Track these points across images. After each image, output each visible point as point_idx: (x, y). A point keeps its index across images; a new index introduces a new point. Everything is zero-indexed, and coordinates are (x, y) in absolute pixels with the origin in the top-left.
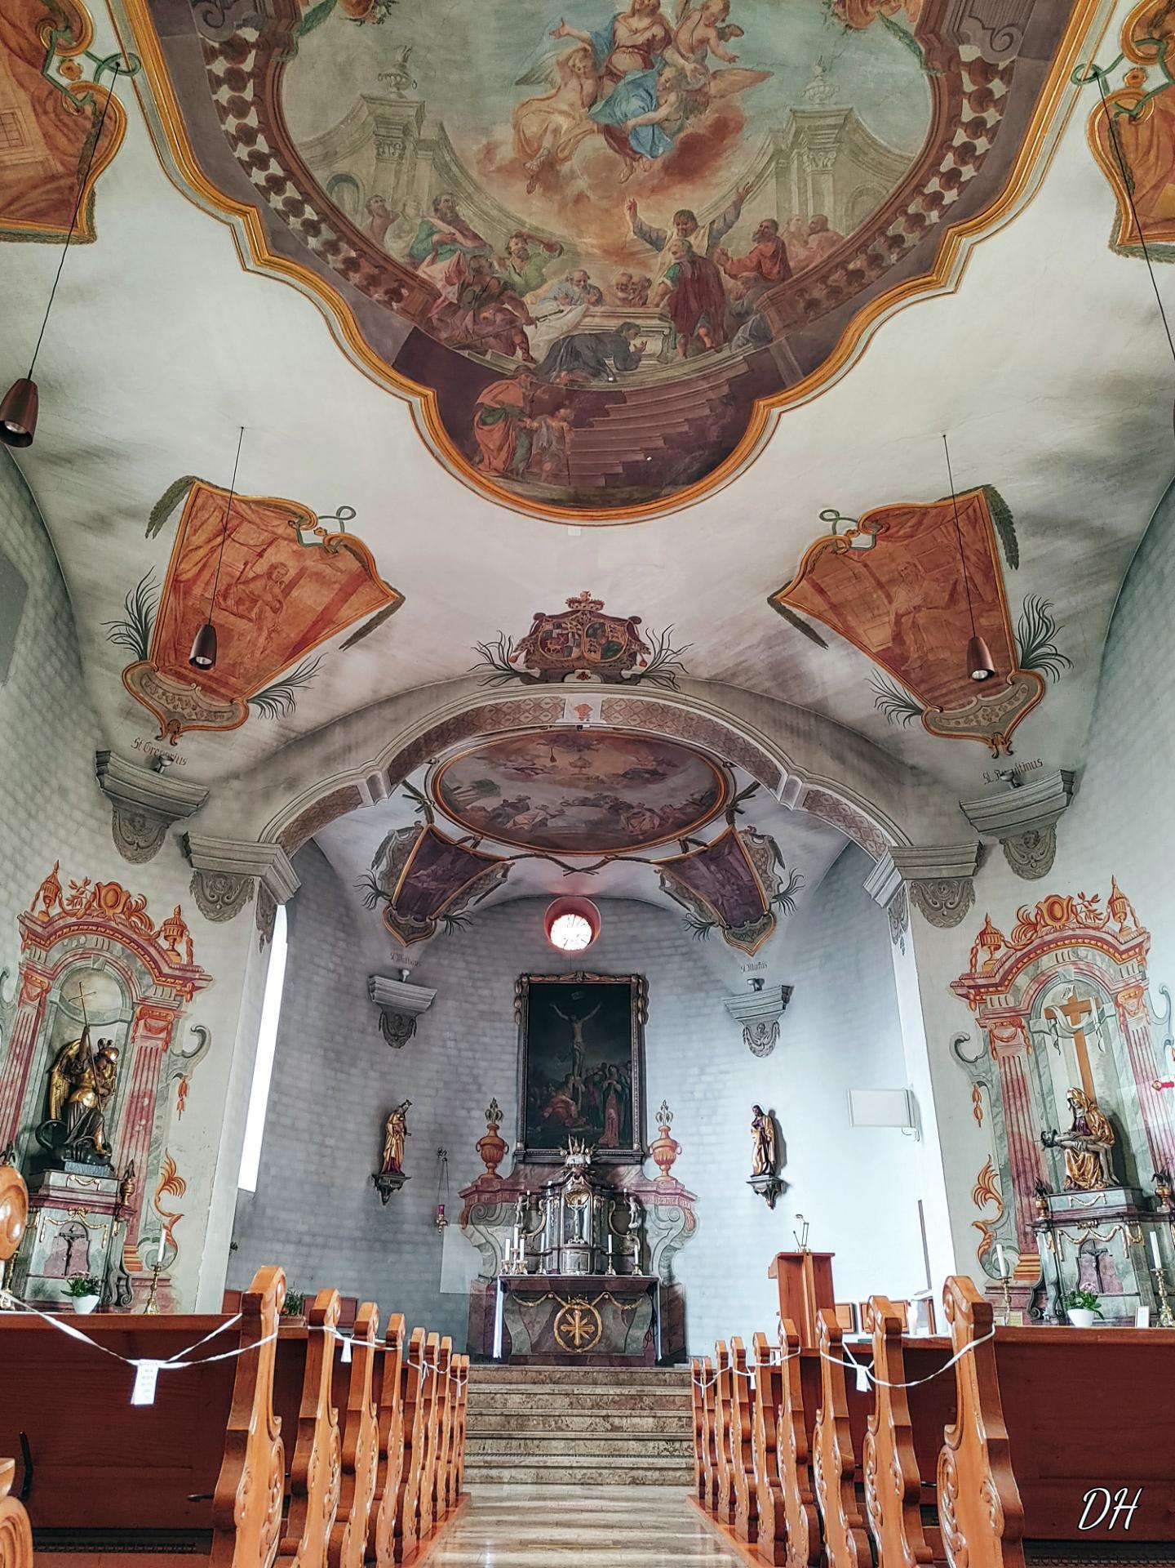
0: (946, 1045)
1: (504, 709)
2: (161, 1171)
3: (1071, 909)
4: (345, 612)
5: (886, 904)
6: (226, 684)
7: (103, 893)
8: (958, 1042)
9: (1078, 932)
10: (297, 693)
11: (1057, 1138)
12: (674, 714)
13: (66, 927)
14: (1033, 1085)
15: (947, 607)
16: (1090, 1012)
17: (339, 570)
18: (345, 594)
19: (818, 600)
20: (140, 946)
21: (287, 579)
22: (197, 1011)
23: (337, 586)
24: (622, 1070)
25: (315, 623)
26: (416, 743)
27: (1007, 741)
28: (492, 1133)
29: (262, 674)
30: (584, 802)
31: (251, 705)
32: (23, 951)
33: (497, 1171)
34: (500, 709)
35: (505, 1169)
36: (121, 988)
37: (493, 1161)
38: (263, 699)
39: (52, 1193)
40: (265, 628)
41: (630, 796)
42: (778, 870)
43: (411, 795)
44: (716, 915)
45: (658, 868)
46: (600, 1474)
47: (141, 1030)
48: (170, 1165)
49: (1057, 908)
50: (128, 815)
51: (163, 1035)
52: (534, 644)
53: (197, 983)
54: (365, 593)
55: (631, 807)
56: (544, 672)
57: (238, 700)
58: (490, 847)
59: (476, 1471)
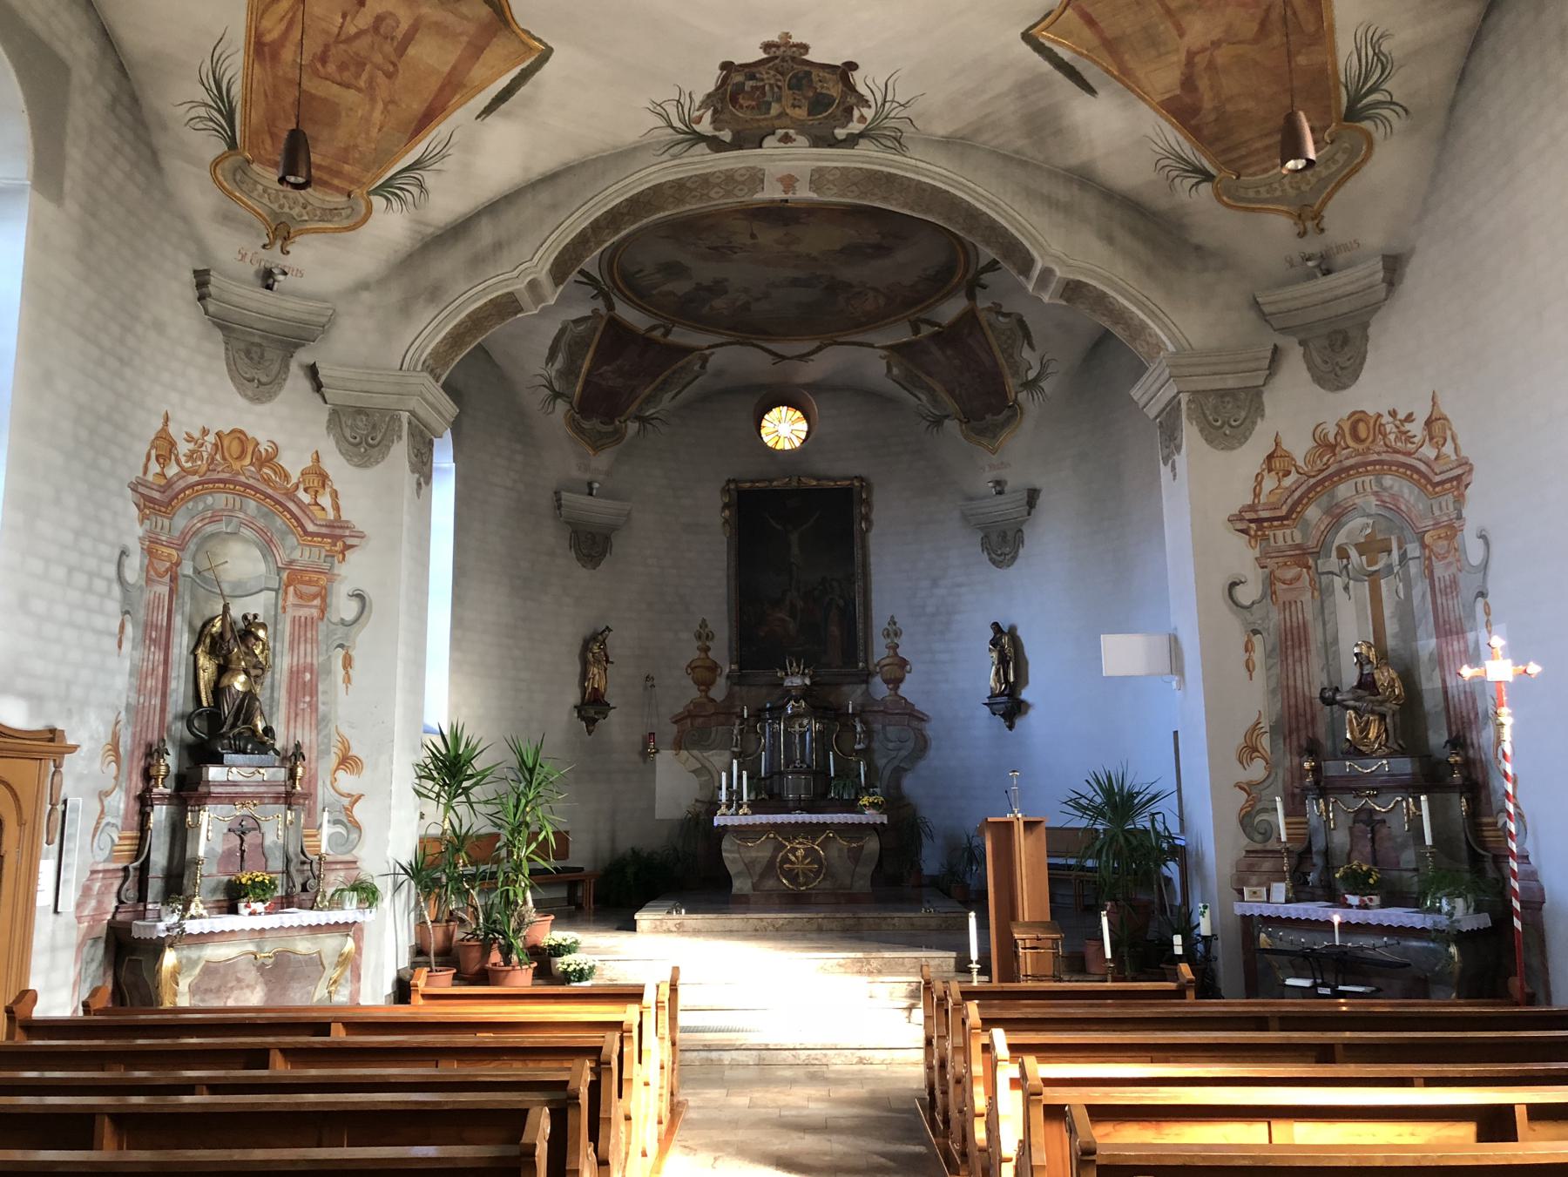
0: (1221, 582)
1: (688, 184)
2: (334, 750)
3: (1379, 429)
4: (478, 72)
5: (1156, 417)
6: (338, 174)
7: (226, 443)
8: (1233, 585)
9: (1384, 457)
10: (429, 179)
11: (1338, 697)
12: (902, 184)
13: (188, 487)
14: (1316, 636)
15: (1256, 41)
16: (1390, 552)
17: (464, 17)
18: (476, 50)
19: (1087, 33)
20: (278, 502)
21: (399, 33)
22: (354, 572)
23: (465, 39)
25: (442, 89)
26: (583, 234)
27: (1318, 216)
28: (703, 655)
29: (384, 157)
30: (795, 282)
31: (372, 197)
32: (142, 523)
34: (684, 185)
35: (719, 691)
36: (261, 551)
37: (705, 684)
38: (387, 189)
39: (213, 789)
40: (378, 98)
41: (848, 274)
42: (1027, 353)
43: (585, 280)
44: (952, 406)
45: (883, 353)
46: (825, 1055)
47: (291, 599)
48: (343, 743)
49: (1362, 427)
50: (242, 346)
51: (317, 602)
52: (722, 100)
53: (350, 541)
54: (498, 49)
55: (851, 286)
56: (736, 135)
57: (357, 192)
58: (681, 336)
59: (695, 1054)
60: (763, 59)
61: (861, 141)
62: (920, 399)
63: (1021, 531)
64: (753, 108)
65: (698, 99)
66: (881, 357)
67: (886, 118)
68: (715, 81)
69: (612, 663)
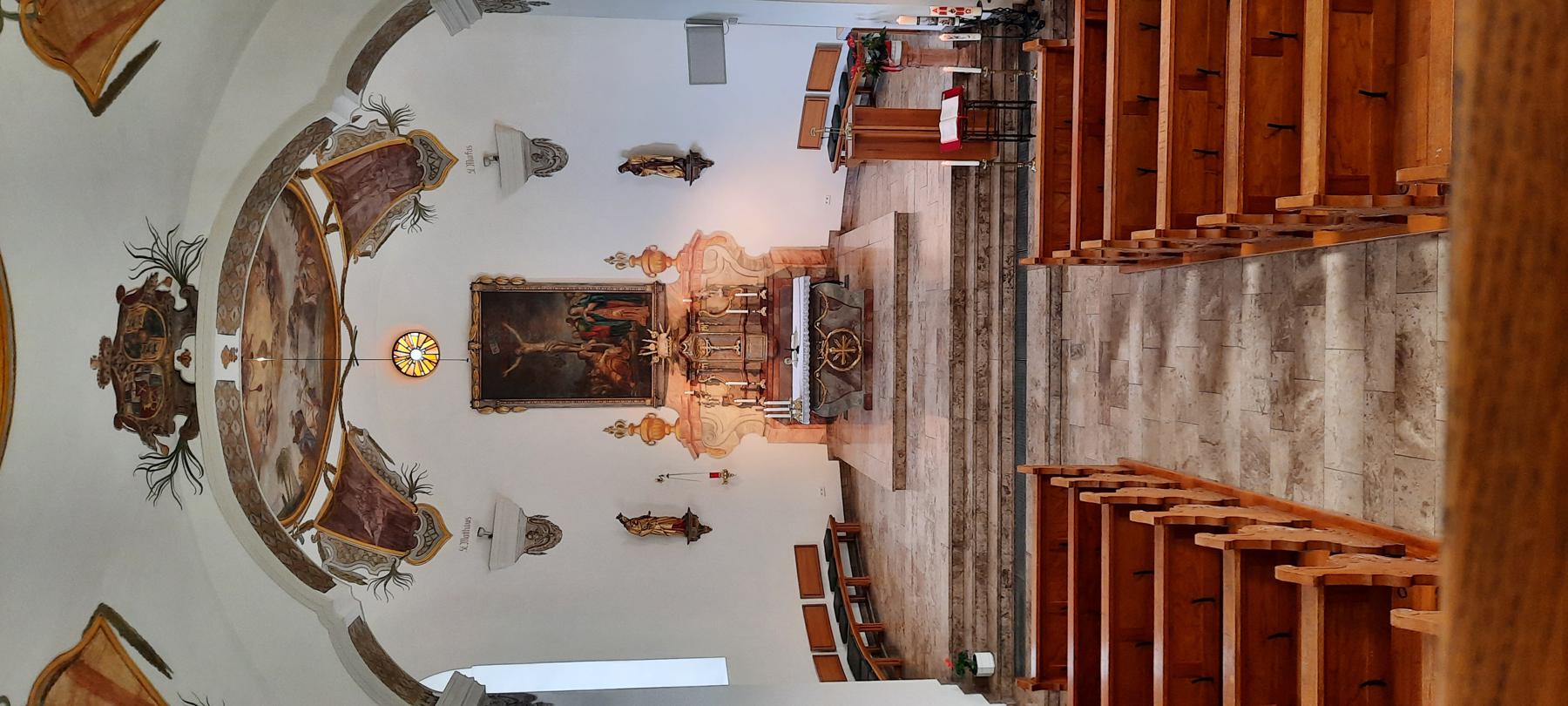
24: (573, 302)
28: (637, 430)
33: (673, 422)
37: (663, 429)
44: (408, 196)
45: (352, 260)
52: (148, 425)
60: (114, 386)
61: (190, 282)
62: (397, 226)
63: (533, 141)
64: (155, 393)
65: (146, 450)
66: (355, 262)
67: (167, 257)
68: (130, 433)
69: (650, 513)
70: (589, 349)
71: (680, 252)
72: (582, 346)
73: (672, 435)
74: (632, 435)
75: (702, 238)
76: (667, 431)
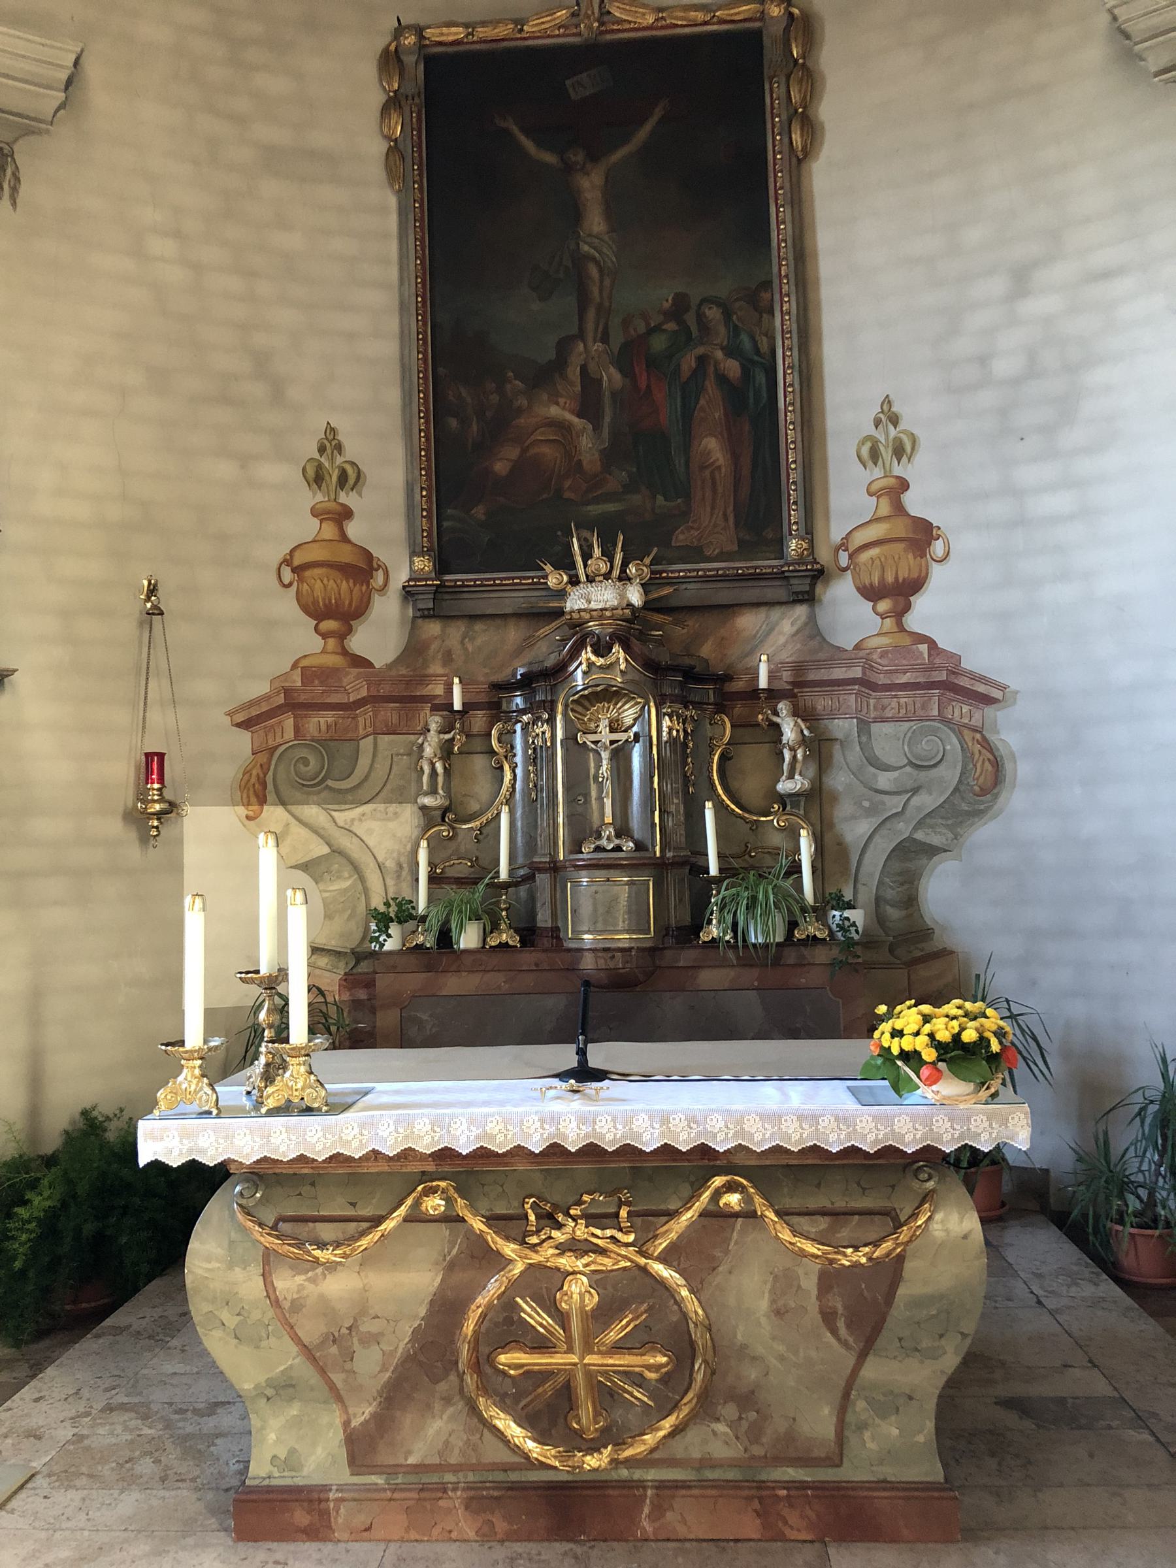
28: (329, 531)
70: (592, 367)
71: (932, 644)
72: (599, 346)
73: (319, 642)
74: (315, 513)
75: (989, 711)
76: (330, 625)
